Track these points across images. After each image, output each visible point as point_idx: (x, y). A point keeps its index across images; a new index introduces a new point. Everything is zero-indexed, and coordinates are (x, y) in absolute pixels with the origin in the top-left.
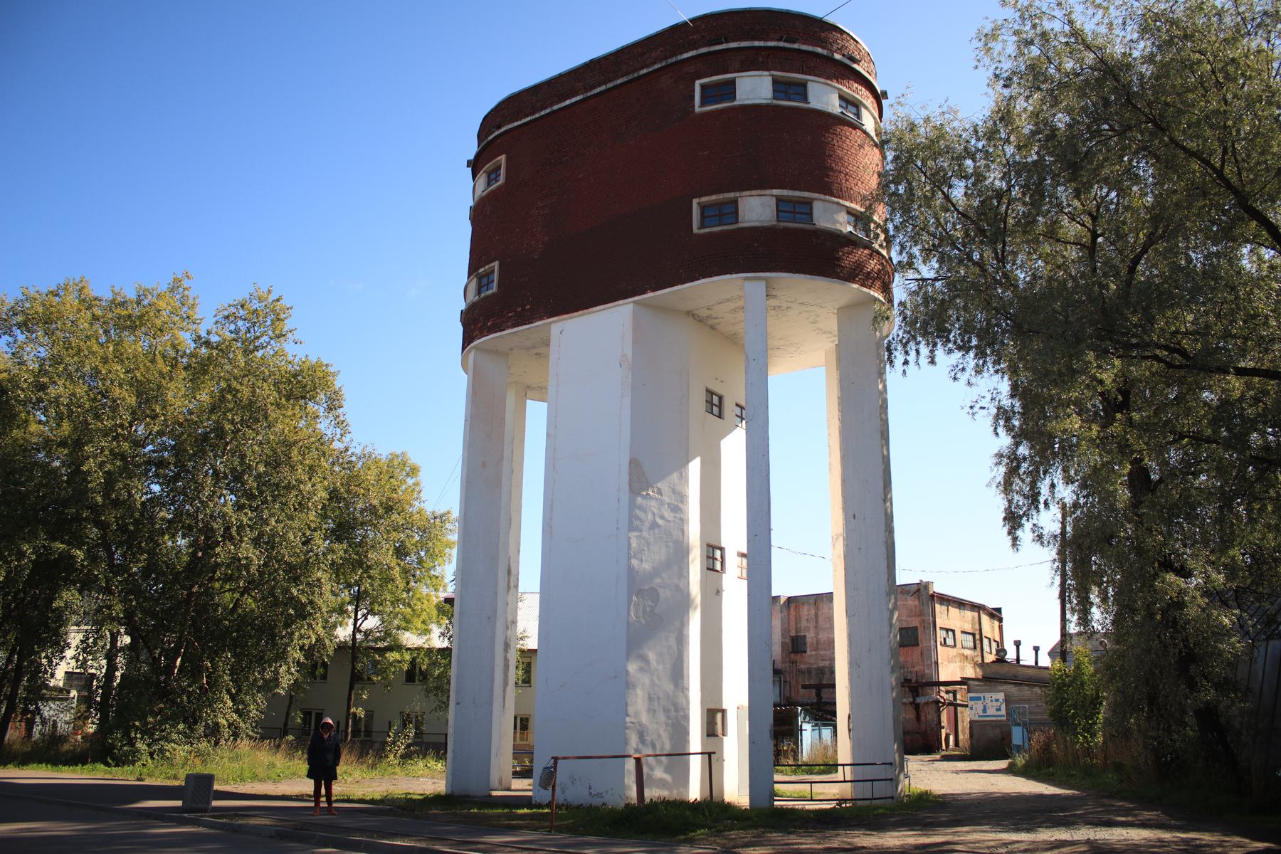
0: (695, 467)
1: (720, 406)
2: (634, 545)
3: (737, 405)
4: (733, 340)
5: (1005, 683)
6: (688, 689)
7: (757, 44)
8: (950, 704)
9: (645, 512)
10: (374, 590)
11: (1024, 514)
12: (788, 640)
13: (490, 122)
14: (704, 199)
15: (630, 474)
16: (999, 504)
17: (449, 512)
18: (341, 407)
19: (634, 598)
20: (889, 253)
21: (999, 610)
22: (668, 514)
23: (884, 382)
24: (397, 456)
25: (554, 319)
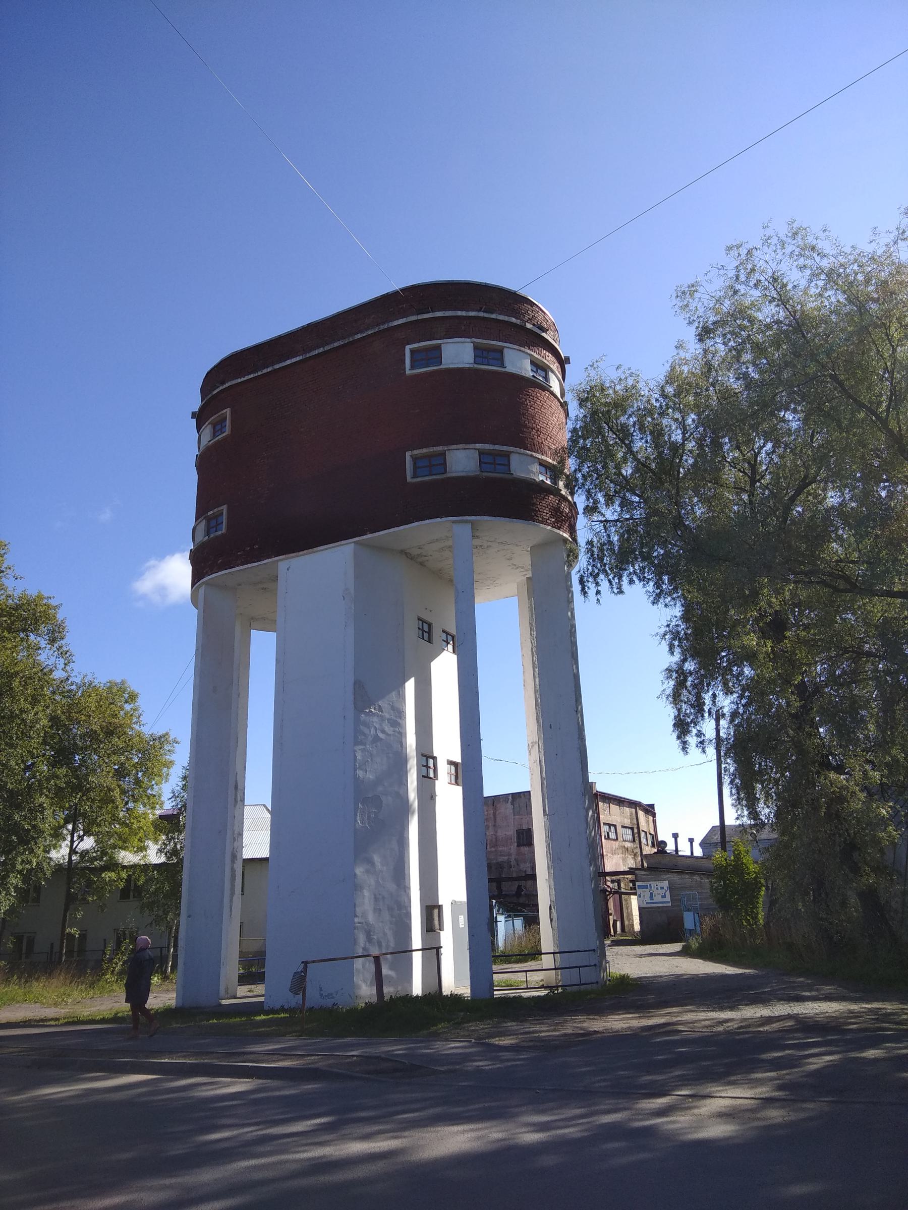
0: (410, 686)
1: (429, 632)
2: (359, 757)
3: (444, 631)
4: (439, 575)
5: (669, 872)
6: (409, 888)
7: (459, 313)
8: (616, 892)
9: (369, 728)
10: (93, 812)
11: (691, 722)
13: (213, 378)
14: (416, 452)
15: (355, 694)
16: (668, 713)
17: (167, 734)
18: (62, 638)
19: (360, 806)
20: (573, 499)
21: (652, 806)
22: (388, 729)
23: (572, 611)
24: (116, 684)
25: (281, 557)
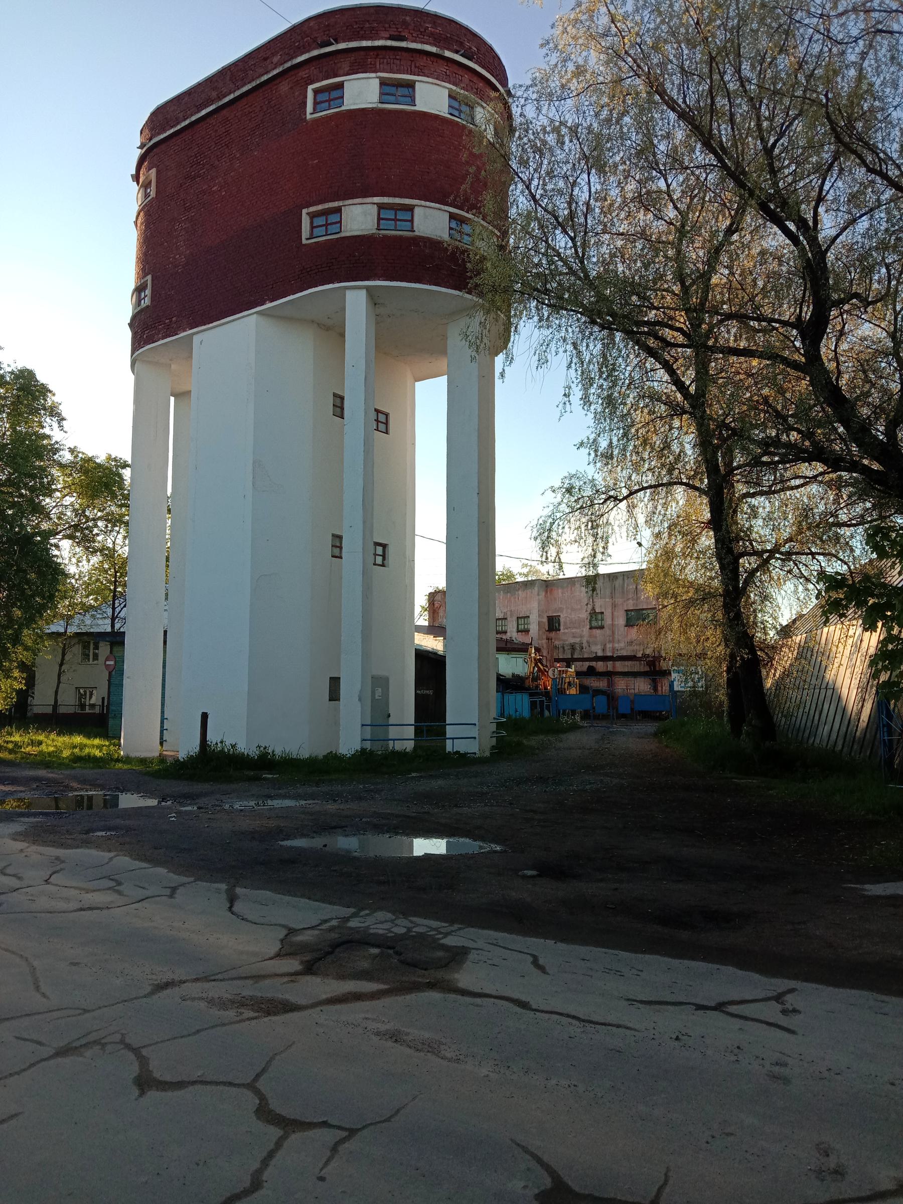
7: (365, 43)
12: (545, 620)
14: (312, 209)
